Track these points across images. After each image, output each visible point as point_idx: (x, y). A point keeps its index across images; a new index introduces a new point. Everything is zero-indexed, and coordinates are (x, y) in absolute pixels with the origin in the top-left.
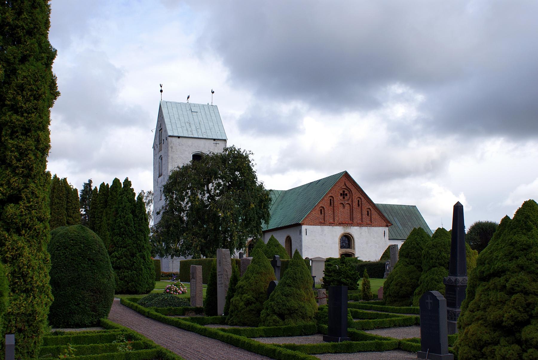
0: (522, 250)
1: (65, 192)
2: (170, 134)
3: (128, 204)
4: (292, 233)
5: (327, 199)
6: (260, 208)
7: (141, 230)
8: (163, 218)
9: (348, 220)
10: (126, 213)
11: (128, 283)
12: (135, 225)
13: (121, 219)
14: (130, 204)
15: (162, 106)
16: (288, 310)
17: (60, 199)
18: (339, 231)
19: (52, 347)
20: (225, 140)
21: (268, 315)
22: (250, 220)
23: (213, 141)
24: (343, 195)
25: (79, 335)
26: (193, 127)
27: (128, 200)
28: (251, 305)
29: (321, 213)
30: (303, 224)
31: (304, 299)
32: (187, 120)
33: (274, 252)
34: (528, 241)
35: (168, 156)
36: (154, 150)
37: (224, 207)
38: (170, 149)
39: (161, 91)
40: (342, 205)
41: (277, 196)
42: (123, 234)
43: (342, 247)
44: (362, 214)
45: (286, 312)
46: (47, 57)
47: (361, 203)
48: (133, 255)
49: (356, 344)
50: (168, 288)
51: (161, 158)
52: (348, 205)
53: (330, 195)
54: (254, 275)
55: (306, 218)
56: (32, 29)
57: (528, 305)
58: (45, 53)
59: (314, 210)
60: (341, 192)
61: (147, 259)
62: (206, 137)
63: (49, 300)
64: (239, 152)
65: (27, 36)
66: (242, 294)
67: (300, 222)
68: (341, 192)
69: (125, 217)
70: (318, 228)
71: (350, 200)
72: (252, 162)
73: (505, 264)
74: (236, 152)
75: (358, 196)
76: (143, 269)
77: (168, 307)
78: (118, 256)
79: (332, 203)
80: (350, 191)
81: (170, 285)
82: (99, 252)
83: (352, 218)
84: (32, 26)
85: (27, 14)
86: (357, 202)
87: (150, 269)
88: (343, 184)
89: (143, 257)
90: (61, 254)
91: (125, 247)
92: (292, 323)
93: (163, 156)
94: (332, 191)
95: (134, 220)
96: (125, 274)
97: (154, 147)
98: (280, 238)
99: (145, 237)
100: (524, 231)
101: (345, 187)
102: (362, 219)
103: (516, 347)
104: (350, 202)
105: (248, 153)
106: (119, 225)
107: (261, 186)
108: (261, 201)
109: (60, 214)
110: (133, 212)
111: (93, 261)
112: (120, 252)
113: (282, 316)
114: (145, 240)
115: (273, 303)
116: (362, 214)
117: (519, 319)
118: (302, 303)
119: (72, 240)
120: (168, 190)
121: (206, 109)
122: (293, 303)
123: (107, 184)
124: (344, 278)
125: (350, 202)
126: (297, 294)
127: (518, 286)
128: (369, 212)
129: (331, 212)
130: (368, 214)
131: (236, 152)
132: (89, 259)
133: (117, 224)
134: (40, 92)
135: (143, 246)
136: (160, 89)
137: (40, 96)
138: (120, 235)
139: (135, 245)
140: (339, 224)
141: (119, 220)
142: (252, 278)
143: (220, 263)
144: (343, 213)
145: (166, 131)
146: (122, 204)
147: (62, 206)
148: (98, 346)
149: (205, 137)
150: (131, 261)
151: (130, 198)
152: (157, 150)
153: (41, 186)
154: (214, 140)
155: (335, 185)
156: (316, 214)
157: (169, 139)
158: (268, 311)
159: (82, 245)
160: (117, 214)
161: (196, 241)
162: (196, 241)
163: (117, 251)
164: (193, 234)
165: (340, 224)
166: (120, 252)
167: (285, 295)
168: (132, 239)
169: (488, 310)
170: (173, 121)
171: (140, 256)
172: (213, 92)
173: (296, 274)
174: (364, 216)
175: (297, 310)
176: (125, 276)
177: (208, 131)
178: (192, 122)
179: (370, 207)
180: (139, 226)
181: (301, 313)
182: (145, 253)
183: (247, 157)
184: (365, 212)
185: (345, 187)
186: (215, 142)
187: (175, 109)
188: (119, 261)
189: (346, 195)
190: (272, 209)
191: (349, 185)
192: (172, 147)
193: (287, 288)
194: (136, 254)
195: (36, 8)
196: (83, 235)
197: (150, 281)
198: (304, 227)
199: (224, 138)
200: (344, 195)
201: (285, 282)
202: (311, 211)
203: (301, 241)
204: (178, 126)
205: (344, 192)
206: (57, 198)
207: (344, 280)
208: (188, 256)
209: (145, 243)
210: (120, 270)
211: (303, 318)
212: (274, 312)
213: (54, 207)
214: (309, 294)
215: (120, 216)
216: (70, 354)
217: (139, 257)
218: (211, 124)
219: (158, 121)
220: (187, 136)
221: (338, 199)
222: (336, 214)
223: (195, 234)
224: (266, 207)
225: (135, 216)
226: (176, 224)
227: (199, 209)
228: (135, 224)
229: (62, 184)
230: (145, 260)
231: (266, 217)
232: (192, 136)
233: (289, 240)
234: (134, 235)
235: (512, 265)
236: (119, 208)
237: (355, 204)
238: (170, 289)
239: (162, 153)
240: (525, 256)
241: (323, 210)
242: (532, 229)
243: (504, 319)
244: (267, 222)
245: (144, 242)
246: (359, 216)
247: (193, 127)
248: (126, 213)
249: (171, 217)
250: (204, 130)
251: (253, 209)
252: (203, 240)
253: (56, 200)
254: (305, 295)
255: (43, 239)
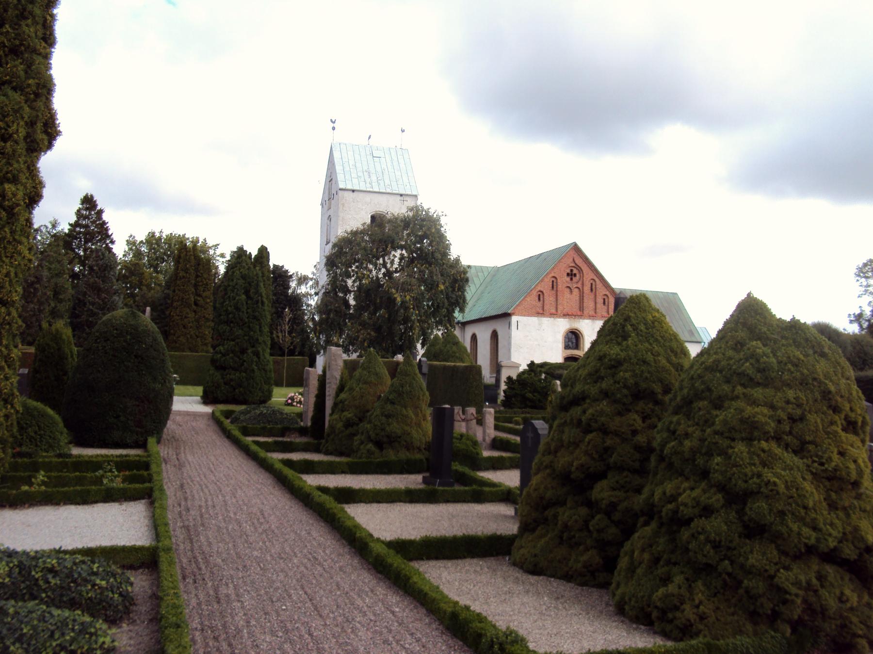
0: (610, 368)
1: (193, 262)
2: (341, 186)
3: (241, 282)
4: (499, 326)
5: (548, 281)
6: (454, 290)
7: (255, 318)
8: (322, 300)
9: (575, 310)
10: (237, 294)
11: (234, 389)
12: (249, 310)
13: (230, 301)
14: (243, 281)
15: (333, 149)
16: (388, 437)
17: (187, 273)
18: (563, 325)
19: (22, 474)
20: (416, 196)
21: (362, 443)
22: (438, 306)
23: (399, 198)
24: (571, 275)
25: (91, 459)
26: (374, 178)
27: (242, 277)
28: (352, 427)
29: (539, 299)
30: (513, 314)
31: (411, 423)
32: (365, 168)
33: (451, 352)
34: (619, 354)
35: (338, 216)
36: (323, 207)
37: (404, 288)
38: (341, 206)
39: (334, 128)
40: (568, 290)
41: (486, 274)
42: (232, 322)
43: (567, 347)
44: (596, 303)
45: (385, 439)
46: (37, 83)
47: (596, 288)
48: (243, 351)
49: (443, 491)
50: (290, 398)
51: (329, 218)
52: (577, 290)
53: (553, 275)
54: (361, 385)
55: (517, 305)
56: (17, 46)
57: (606, 449)
58: (34, 78)
59: (529, 294)
60: (569, 271)
61: (262, 357)
62: (390, 192)
63: (12, 411)
64: (427, 212)
65: (10, 57)
66: (343, 411)
67: (509, 312)
68: (569, 271)
69: (235, 299)
70: (534, 320)
71: (580, 282)
72: (445, 227)
73: (587, 387)
74: (424, 213)
75: (592, 277)
76: (256, 371)
77: (262, 425)
78: (223, 351)
79: (555, 287)
80: (580, 270)
81: (293, 394)
82: (151, 346)
83: (581, 308)
84: (17, 42)
85: (10, 27)
86: (590, 286)
87: (265, 371)
88: (571, 260)
89: (257, 354)
90: (100, 348)
91: (233, 340)
92: (391, 455)
93: (332, 216)
94: (555, 270)
95: (247, 303)
96: (231, 377)
97: (322, 204)
98: (483, 334)
99: (260, 327)
100: (620, 339)
101: (573, 265)
102: (595, 309)
103: (583, 511)
104: (579, 285)
105: (440, 214)
106: (227, 310)
107: (457, 260)
108: (455, 281)
109: (186, 292)
110: (247, 293)
111: (142, 359)
112: (226, 347)
113: (379, 445)
114: (260, 331)
115: (369, 426)
116: (596, 303)
117: (591, 469)
118: (407, 428)
119: (116, 329)
120: (331, 262)
121: (393, 153)
122: (395, 427)
123: (250, 253)
124: (530, 392)
125: (579, 285)
126: (402, 415)
127: (596, 421)
128: (606, 300)
129: (552, 299)
130: (604, 303)
131: (424, 213)
132: (136, 356)
133: (225, 309)
134: (10, 131)
135: (257, 340)
136: (335, 125)
137: (11, 136)
138: (228, 322)
139: (246, 338)
140: (564, 315)
141: (227, 303)
142: (358, 389)
143: (329, 367)
144: (569, 300)
145: (337, 182)
146: (232, 280)
147: (189, 281)
148: (86, 476)
149: (388, 191)
150: (240, 359)
151: (243, 273)
152: (326, 207)
153: (7, 257)
154: (401, 195)
155: (559, 262)
156: (532, 300)
157: (340, 193)
158: (363, 437)
159: (129, 337)
160: (226, 294)
161: (363, 334)
162: (363, 334)
163: (223, 345)
164: (360, 324)
165: (565, 315)
166: (226, 347)
167: (386, 416)
168: (242, 330)
169: (559, 454)
170: (347, 169)
171: (253, 352)
172: (403, 131)
173: (402, 387)
174: (598, 306)
175: (400, 437)
176: (231, 380)
177: (394, 184)
178: (372, 170)
179: (607, 293)
180: (253, 312)
181: (406, 441)
182: (259, 349)
183: (438, 220)
184: (600, 300)
185: (573, 265)
186: (402, 198)
187: (350, 153)
188: (224, 358)
189: (575, 275)
190: (470, 292)
191: (579, 262)
192: (343, 205)
193: (389, 407)
194: (247, 349)
195: (26, 18)
196: (132, 323)
197: (266, 387)
198: (514, 319)
199: (414, 193)
200: (572, 275)
201: (388, 398)
202: (526, 297)
203: (510, 337)
204: (354, 175)
205: (572, 271)
206: (182, 270)
207: (529, 395)
208: (352, 353)
209: (261, 336)
210: (225, 370)
211: (408, 449)
212: (370, 439)
213: (178, 282)
214: (420, 415)
215: (229, 297)
216: (39, 485)
217: (252, 355)
218: (398, 173)
219: (328, 169)
220: (365, 189)
221: (564, 280)
222: (559, 301)
223: (364, 325)
224: (462, 289)
225: (249, 297)
226: (338, 309)
227: (369, 290)
228: (248, 308)
229: (190, 251)
230: (259, 358)
231: (460, 302)
232: (371, 190)
233: (495, 336)
234: (246, 323)
235: (594, 390)
236: (229, 286)
237: (587, 289)
238: (292, 399)
239: (331, 212)
240: (613, 376)
241: (541, 296)
242: (630, 336)
243: (573, 469)
244: (462, 310)
245: (259, 333)
246: (592, 305)
247: (374, 178)
248: (237, 294)
249: (332, 300)
250: (387, 182)
251: (442, 291)
252: (373, 333)
253: (182, 274)
254: (413, 417)
255: (4, 328)
